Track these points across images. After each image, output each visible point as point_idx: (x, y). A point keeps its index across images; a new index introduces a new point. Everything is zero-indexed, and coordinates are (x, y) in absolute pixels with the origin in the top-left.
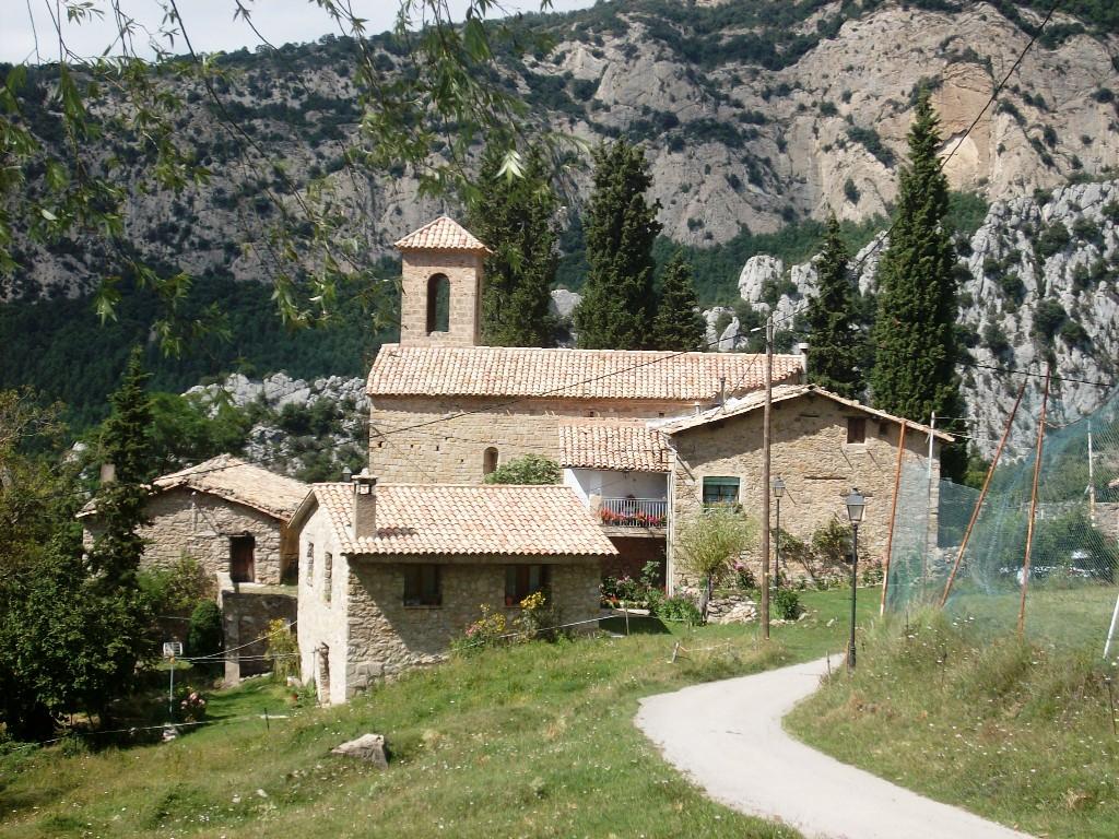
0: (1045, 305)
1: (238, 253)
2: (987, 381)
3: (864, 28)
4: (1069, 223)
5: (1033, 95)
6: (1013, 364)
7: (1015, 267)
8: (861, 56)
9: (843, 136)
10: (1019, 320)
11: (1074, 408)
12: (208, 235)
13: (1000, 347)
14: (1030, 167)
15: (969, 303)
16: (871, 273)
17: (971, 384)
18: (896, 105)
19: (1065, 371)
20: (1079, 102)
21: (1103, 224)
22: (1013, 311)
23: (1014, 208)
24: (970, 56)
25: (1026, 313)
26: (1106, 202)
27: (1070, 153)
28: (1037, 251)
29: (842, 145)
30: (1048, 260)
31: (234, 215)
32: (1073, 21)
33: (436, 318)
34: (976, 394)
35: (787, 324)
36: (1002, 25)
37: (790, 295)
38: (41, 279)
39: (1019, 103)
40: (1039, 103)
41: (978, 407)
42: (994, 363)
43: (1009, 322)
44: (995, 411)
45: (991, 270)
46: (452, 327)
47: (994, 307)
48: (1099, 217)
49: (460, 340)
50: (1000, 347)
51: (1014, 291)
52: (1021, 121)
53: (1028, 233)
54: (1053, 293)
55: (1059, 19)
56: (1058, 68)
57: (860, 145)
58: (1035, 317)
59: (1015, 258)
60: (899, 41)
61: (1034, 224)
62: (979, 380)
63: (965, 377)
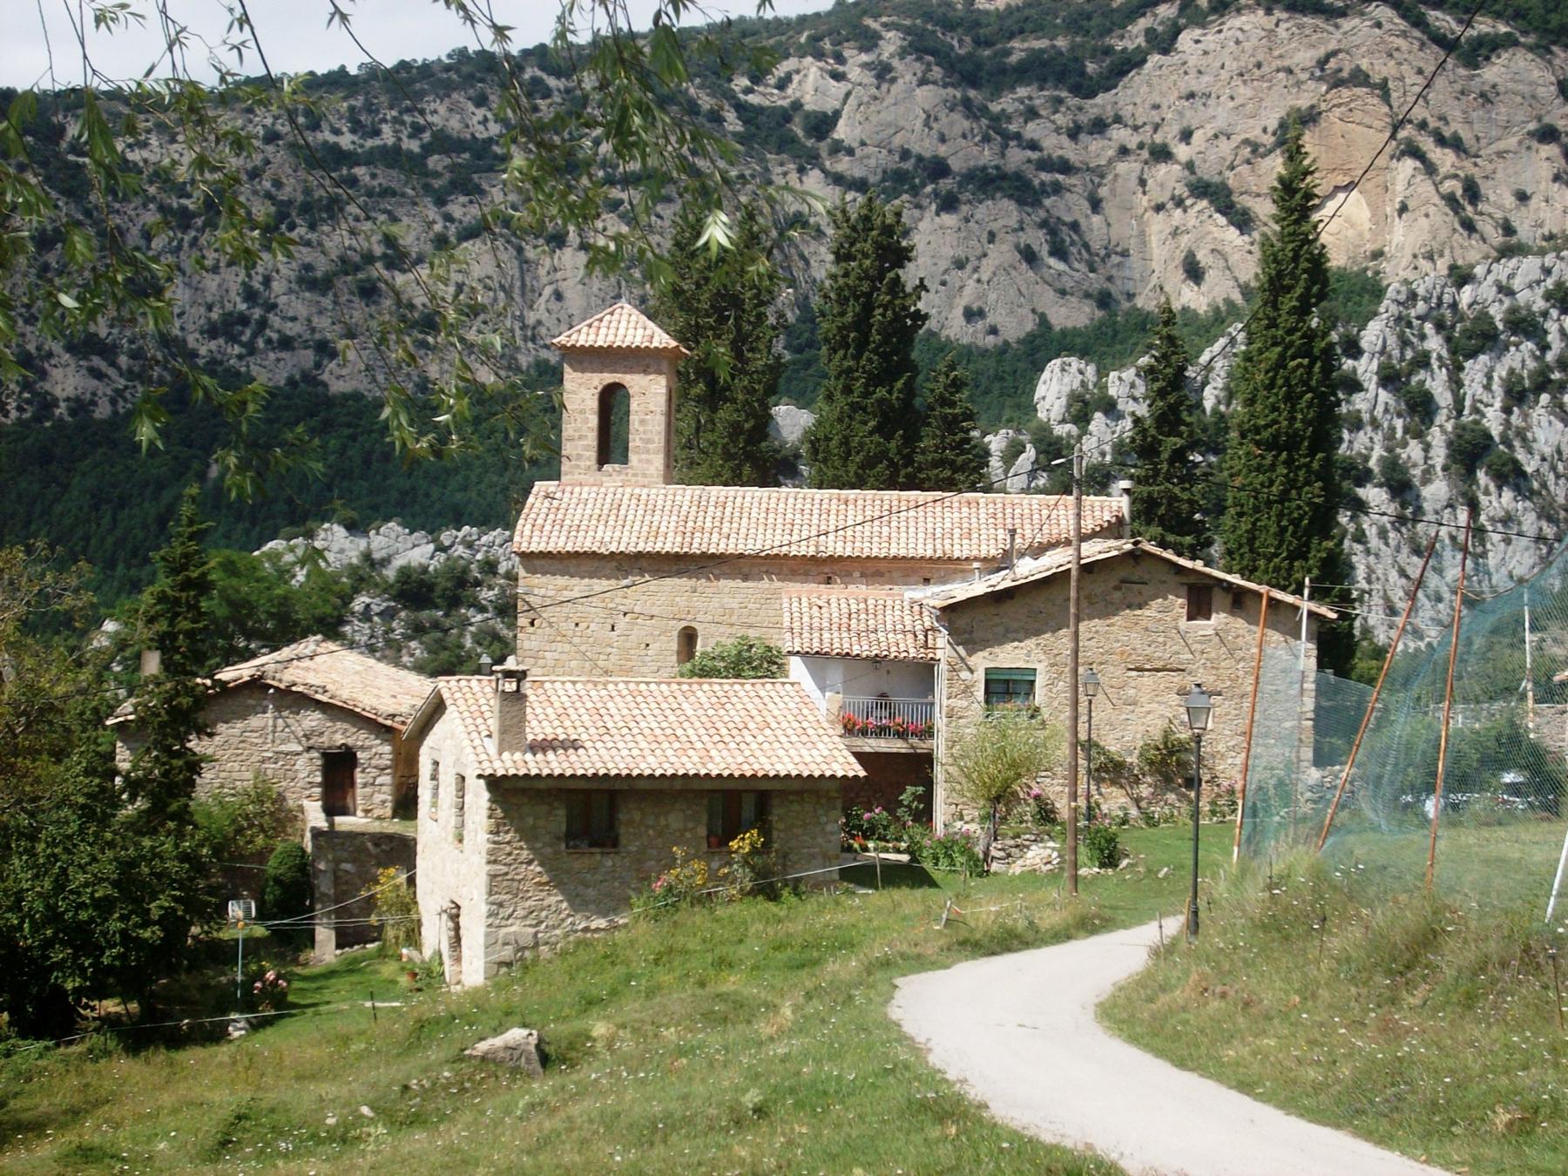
0: (1464, 428)
1: (333, 355)
2: (1383, 534)
3: (1210, 39)
4: (1497, 312)
5: (1447, 133)
6: (1419, 510)
7: (1422, 375)
8: (1205, 79)
9: (1182, 190)
10: (1427, 448)
11: (1504, 571)
12: (291, 329)
13: (1401, 486)
14: (1443, 234)
15: (1357, 424)
16: (1220, 383)
17: (1360, 537)
18: (1255, 147)
19: (1492, 520)
20: (1511, 142)
21: (1545, 314)
22: (1419, 436)
23: (1421, 291)
24: (1359, 78)
25: (1437, 438)
26: (1550, 283)
27: (1499, 215)
28: (1453, 352)
29: (1179, 203)
30: (1468, 364)
31: (327, 302)
32: (1503, 29)
33: (611, 447)
34: (1368, 552)
35: (1103, 454)
36: (1404, 34)
37: (1106, 413)
38: (58, 392)
39: (1427, 144)
40: (1456, 144)
41: (1370, 571)
42: (1392, 508)
43: (1414, 450)
44: (1393, 575)
45: (1389, 378)
46: (632, 457)
47: (1393, 429)
48: (1539, 304)
49: (645, 476)
50: (1401, 486)
51: (1421, 408)
52: (1430, 169)
53: (1440, 326)
54: (1475, 410)
55: (1484, 26)
56: (1483, 95)
57: (1204, 203)
58: (1450, 444)
59: (1422, 361)
60: (1260, 57)
61: (1448, 313)
62: (1372, 533)
63: (1351, 528)
